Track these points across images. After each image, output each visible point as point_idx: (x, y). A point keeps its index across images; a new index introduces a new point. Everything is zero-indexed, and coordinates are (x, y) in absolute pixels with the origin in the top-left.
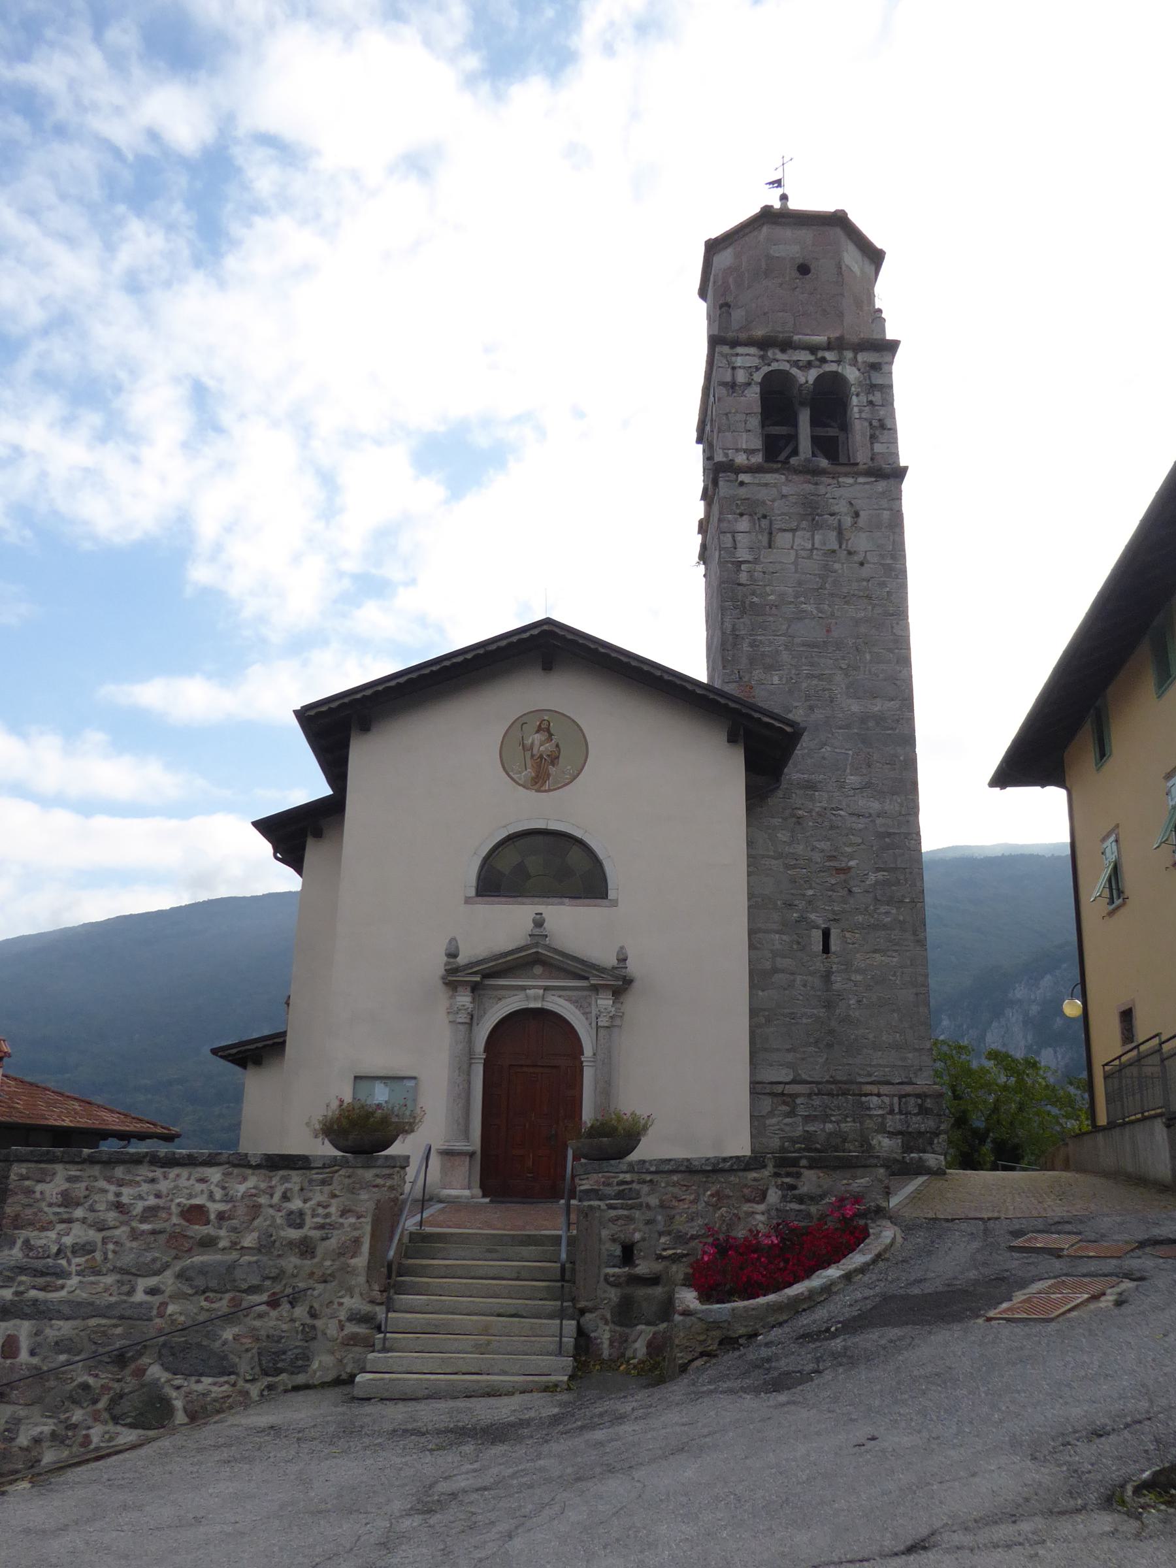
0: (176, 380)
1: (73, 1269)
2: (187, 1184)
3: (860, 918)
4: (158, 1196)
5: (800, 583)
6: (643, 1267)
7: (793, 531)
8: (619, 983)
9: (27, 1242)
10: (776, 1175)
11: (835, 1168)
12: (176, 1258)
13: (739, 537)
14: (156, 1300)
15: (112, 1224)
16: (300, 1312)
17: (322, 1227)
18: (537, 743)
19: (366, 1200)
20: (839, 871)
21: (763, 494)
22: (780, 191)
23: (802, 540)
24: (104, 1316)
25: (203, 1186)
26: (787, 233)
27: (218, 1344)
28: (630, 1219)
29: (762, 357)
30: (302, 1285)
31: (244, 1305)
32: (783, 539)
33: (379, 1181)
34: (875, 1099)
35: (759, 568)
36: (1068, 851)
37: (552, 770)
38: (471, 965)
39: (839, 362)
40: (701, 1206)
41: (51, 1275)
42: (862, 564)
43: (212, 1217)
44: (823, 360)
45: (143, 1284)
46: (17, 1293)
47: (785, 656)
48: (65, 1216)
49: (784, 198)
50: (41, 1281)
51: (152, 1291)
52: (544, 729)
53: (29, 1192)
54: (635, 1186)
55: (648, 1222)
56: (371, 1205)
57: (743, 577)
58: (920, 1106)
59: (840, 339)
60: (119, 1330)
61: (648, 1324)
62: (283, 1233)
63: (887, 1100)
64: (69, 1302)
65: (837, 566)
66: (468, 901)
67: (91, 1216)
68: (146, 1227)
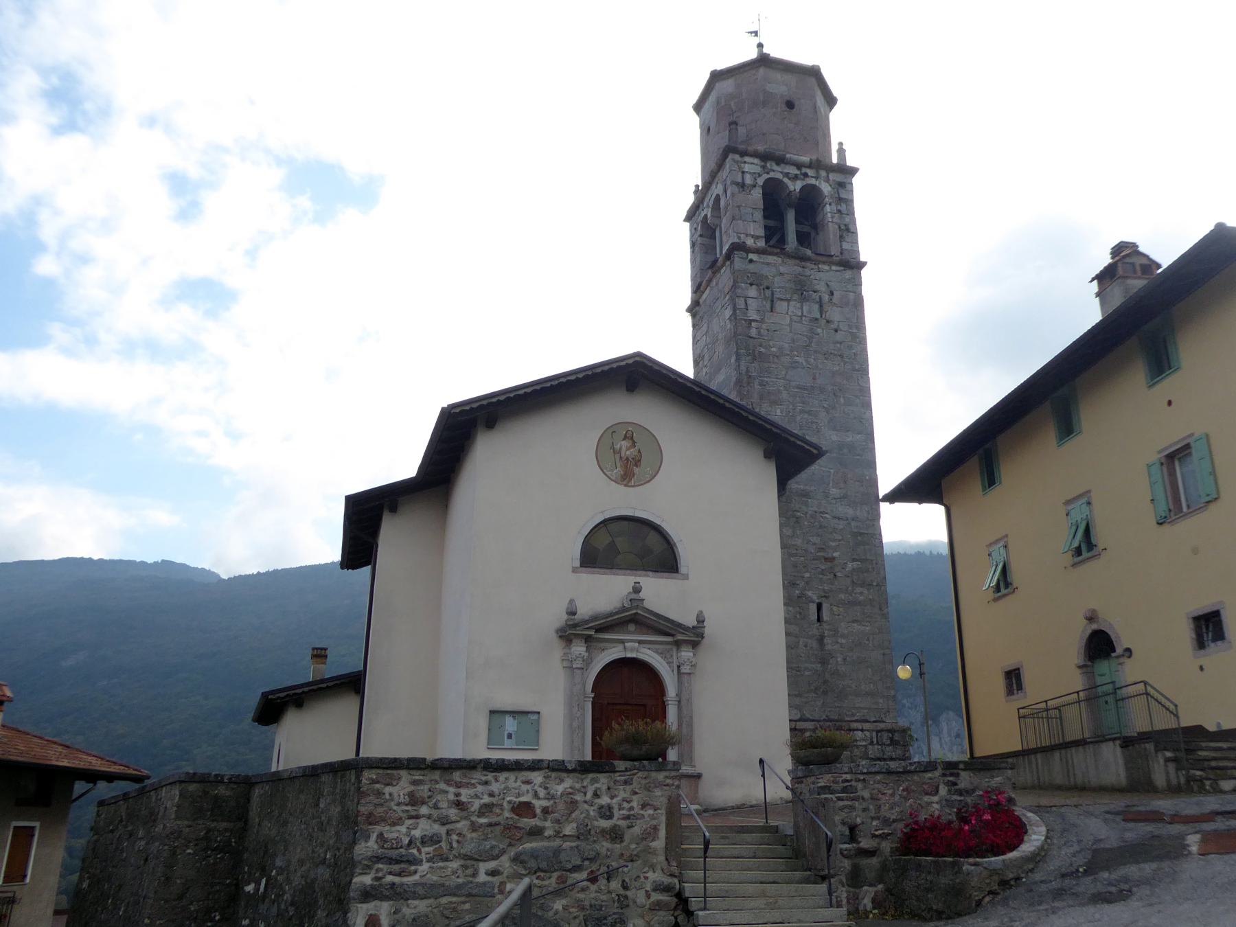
0: (44, 72)
1: (423, 856)
2: (514, 785)
3: (842, 596)
4: (491, 795)
5: (793, 341)
6: (865, 843)
7: (788, 301)
8: (690, 636)
9: (381, 835)
10: (944, 775)
11: (981, 770)
12: (510, 845)
13: (750, 301)
14: (496, 880)
15: (453, 819)
16: (615, 885)
17: (627, 817)
18: (624, 448)
19: (660, 797)
20: (826, 559)
21: (765, 271)
22: (756, 40)
23: (794, 308)
24: (455, 895)
25: (529, 787)
26: (778, 76)
27: (551, 913)
28: (852, 808)
29: (764, 167)
30: (615, 865)
31: (570, 882)
32: (781, 306)
33: (668, 781)
34: (860, 733)
35: (764, 326)
36: (945, 551)
37: (636, 470)
38: (586, 622)
39: (817, 178)
40: (897, 798)
41: (404, 862)
42: (836, 331)
43: (538, 811)
44: (806, 175)
45: (484, 867)
46: (377, 879)
47: (785, 395)
48: (414, 813)
49: (760, 46)
50: (396, 868)
51: (493, 873)
52: (629, 437)
53: (379, 794)
54: (853, 783)
55: (864, 810)
56: (664, 800)
57: (753, 332)
58: (892, 739)
59: (818, 161)
60: (467, 906)
61: (871, 885)
62: (596, 823)
63: (868, 734)
64: (423, 885)
65: (819, 330)
66: (574, 570)
67: (435, 813)
68: (483, 821)
